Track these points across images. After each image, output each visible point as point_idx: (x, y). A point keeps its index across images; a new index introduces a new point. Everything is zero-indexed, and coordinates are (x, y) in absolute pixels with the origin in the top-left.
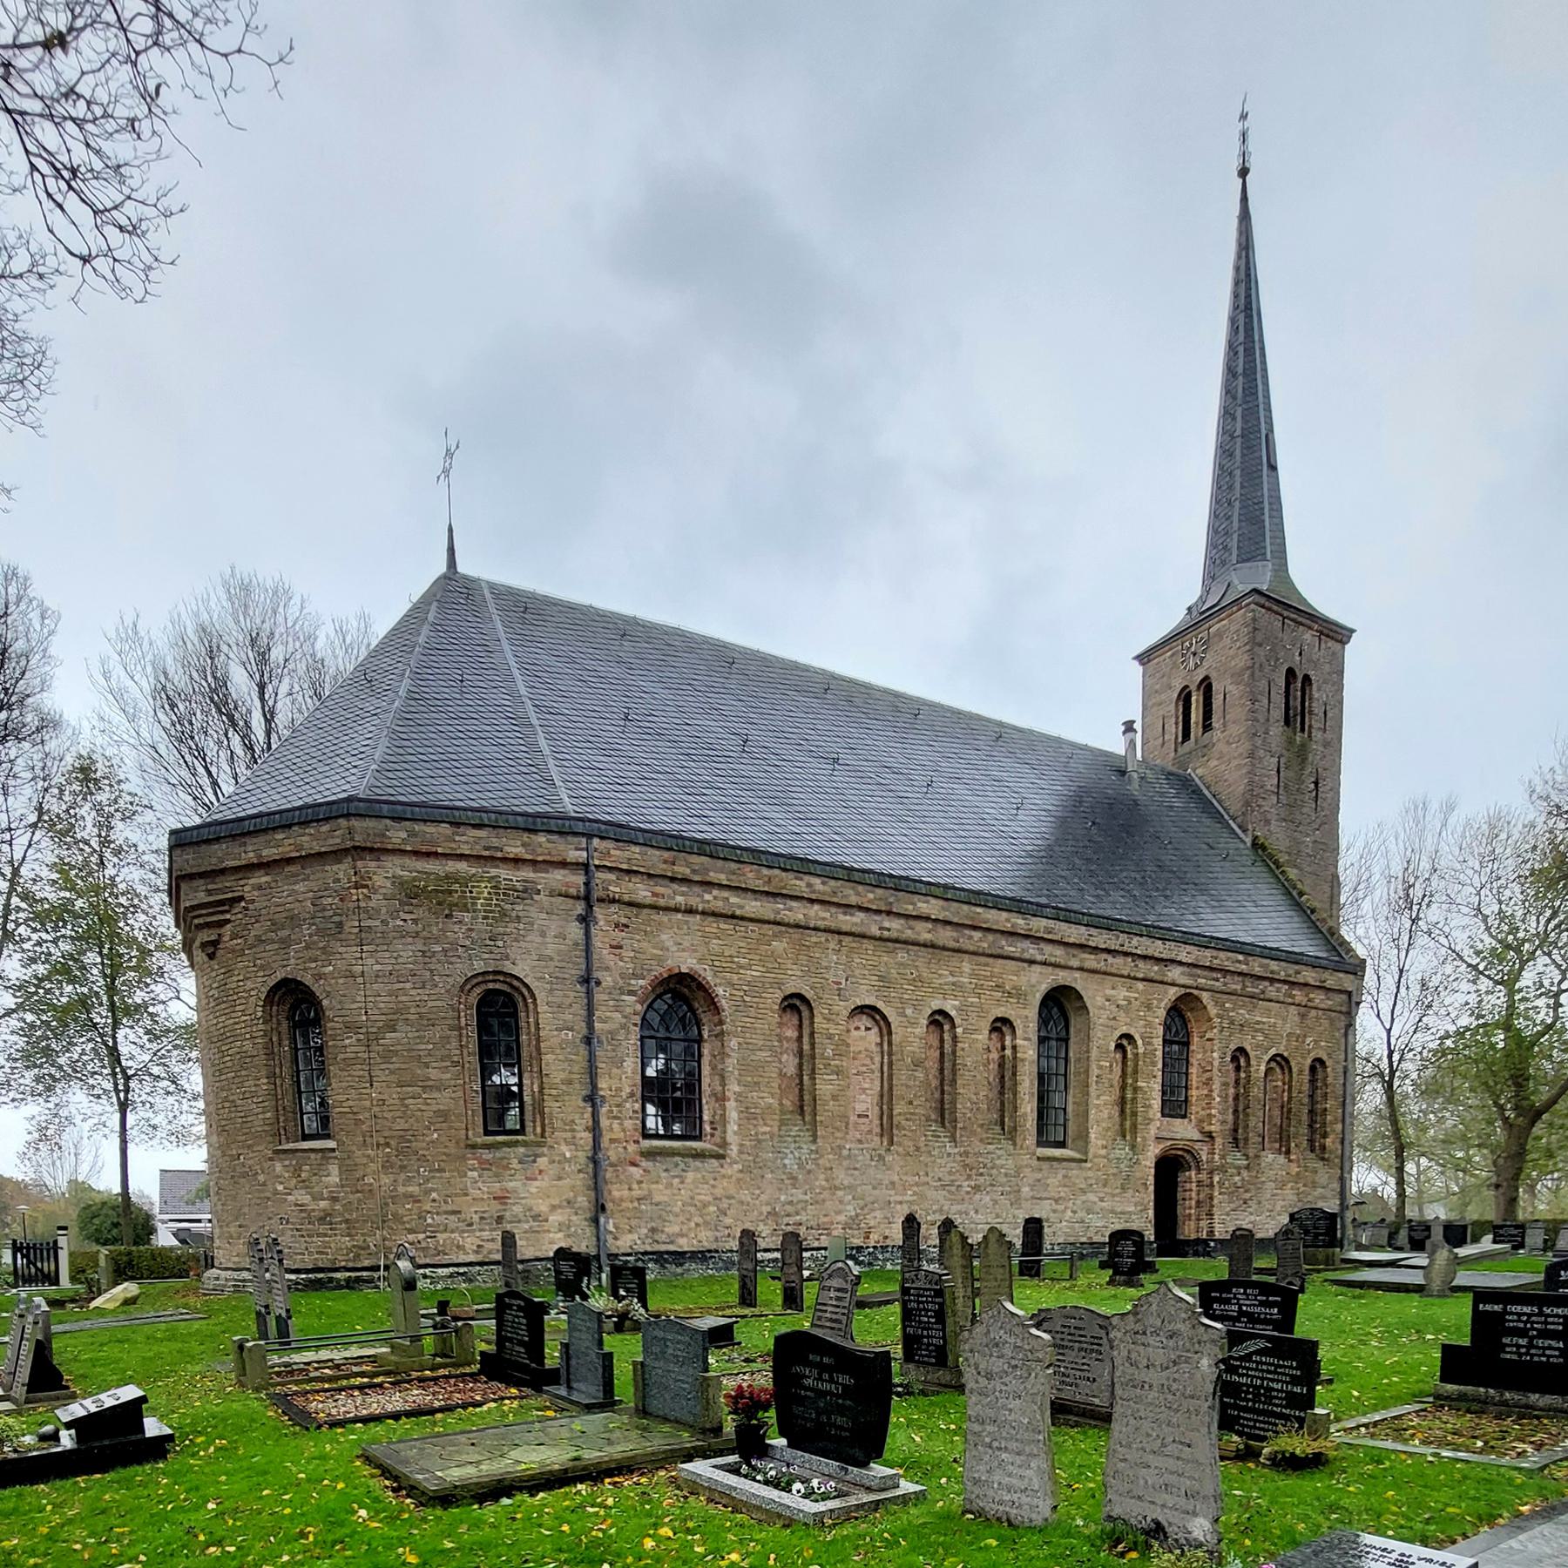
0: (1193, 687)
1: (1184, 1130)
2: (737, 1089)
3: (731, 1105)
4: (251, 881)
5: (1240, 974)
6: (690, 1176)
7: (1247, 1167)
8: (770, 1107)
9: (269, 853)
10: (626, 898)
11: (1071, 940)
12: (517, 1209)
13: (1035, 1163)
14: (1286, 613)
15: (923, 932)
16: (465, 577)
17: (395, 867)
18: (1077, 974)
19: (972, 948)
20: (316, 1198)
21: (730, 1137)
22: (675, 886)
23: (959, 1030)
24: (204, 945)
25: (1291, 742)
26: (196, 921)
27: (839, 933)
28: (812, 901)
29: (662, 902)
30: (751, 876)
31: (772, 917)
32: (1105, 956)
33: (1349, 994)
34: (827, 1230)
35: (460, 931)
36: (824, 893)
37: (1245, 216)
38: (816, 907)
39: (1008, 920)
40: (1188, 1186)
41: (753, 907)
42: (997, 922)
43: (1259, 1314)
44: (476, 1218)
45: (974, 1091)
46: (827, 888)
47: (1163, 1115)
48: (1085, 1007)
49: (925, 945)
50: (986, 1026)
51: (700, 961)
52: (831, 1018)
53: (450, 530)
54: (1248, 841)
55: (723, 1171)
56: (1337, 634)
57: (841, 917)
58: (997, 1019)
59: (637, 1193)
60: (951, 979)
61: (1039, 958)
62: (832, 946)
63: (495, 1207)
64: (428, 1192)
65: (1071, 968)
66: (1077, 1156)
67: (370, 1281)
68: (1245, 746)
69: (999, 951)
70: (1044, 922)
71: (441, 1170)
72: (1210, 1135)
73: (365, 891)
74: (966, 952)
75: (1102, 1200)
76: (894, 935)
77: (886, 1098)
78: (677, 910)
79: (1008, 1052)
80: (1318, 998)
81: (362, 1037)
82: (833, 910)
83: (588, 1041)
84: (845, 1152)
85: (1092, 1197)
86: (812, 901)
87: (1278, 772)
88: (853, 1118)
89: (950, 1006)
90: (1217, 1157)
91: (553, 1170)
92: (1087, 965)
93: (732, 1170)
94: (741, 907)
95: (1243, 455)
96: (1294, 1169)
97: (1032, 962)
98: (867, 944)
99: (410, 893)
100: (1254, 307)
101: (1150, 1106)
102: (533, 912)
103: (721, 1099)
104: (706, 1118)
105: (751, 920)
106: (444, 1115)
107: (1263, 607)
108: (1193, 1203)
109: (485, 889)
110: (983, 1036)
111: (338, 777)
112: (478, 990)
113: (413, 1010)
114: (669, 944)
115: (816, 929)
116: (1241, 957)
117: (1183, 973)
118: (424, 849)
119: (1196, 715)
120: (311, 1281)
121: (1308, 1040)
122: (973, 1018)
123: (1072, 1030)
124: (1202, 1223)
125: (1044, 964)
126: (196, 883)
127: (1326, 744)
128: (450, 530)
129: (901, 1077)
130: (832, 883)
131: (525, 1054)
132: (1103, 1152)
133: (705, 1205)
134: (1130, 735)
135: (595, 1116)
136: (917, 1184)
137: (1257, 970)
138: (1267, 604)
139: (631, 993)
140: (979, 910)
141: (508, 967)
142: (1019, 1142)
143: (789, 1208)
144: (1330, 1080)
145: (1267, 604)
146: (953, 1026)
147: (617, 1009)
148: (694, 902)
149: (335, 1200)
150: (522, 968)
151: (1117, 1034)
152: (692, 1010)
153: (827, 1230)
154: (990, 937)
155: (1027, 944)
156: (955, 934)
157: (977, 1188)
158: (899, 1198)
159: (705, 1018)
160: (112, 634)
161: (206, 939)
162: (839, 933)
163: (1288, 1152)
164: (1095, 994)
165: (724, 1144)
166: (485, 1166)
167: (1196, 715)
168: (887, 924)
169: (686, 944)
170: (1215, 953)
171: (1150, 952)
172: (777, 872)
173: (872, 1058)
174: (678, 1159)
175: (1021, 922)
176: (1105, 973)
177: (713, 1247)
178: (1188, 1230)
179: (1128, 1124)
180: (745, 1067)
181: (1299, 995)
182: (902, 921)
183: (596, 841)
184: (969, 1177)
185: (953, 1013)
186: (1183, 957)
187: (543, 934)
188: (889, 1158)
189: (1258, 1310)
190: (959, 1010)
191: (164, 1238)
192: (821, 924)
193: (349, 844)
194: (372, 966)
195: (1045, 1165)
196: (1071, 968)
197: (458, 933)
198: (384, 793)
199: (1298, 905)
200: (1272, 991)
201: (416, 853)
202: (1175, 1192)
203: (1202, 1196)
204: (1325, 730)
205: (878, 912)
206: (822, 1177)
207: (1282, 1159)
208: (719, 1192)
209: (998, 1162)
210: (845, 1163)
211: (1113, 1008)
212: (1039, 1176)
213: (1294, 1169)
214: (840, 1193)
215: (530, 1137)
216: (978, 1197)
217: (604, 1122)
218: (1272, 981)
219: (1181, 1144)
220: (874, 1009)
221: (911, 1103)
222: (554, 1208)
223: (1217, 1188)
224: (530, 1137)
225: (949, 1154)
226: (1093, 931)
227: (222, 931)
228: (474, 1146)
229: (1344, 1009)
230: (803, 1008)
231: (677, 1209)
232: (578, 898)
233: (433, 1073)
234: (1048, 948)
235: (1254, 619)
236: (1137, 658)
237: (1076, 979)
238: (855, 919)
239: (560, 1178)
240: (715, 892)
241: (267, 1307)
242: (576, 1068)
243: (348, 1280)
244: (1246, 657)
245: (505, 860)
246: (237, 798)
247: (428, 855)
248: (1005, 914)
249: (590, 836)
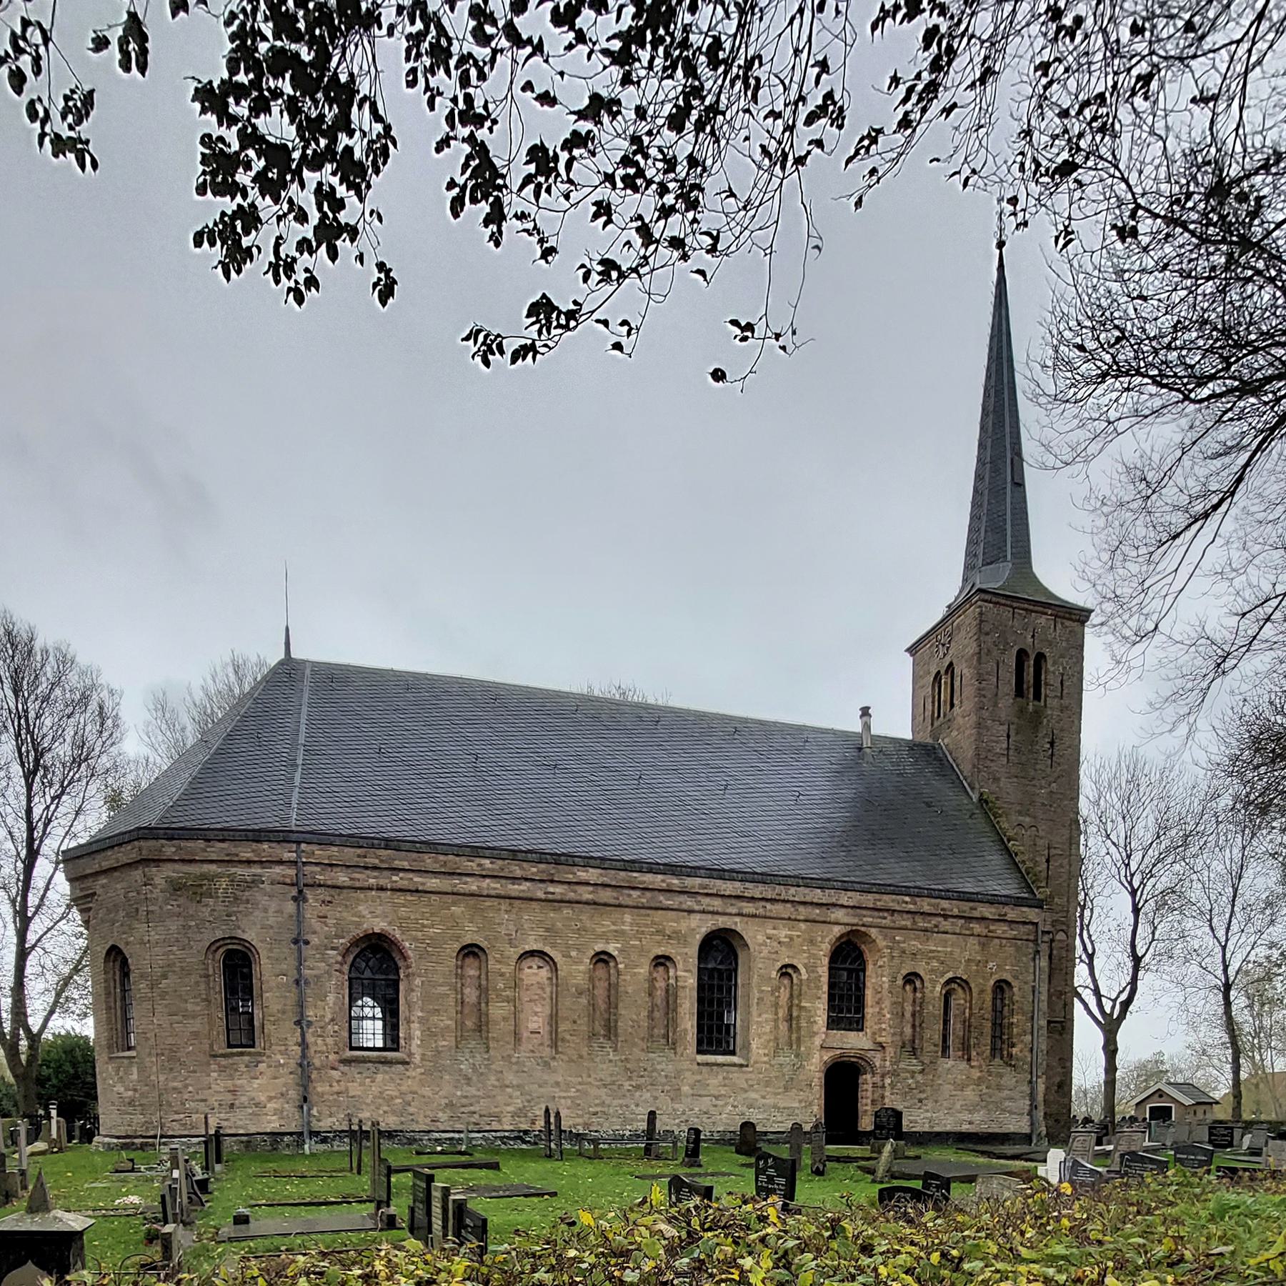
1: (854, 1041)
2: (420, 1014)
3: (415, 1026)
5: (908, 912)
6: (379, 1077)
7: (922, 1072)
8: (448, 1027)
9: (106, 865)
10: (329, 883)
11: (727, 893)
12: (244, 1099)
13: (696, 1067)
14: (1015, 605)
17: (169, 871)
18: (737, 919)
19: (631, 903)
20: (127, 1089)
21: (414, 1049)
22: (368, 872)
23: (621, 966)
25: (1022, 711)
27: (510, 898)
28: (484, 876)
29: (357, 884)
30: (429, 861)
31: (449, 889)
32: (763, 903)
34: (498, 1117)
35: (206, 911)
36: (493, 870)
37: (1001, 280)
38: (488, 881)
39: (663, 881)
41: (433, 883)
42: (653, 883)
44: (216, 1104)
45: (632, 1014)
51: (390, 923)
52: (501, 962)
54: (975, 797)
55: (408, 1074)
57: (510, 886)
59: (336, 1088)
60: (613, 928)
61: (697, 908)
62: (503, 908)
63: (229, 1097)
64: (186, 1086)
65: (730, 914)
67: (153, 1145)
68: (974, 718)
69: (658, 905)
70: (698, 881)
71: (194, 1072)
72: (882, 1047)
74: (627, 907)
75: (764, 1097)
76: (559, 897)
77: (554, 1019)
78: (371, 889)
79: (672, 981)
80: (1001, 929)
82: (503, 881)
83: (297, 982)
84: (514, 1060)
85: (753, 1095)
86: (484, 876)
87: (1008, 736)
89: (612, 948)
90: (888, 1063)
91: (270, 1072)
92: (745, 911)
94: (423, 884)
95: (991, 477)
96: (976, 1074)
97: (690, 911)
98: (534, 905)
99: (176, 888)
100: (1005, 355)
102: (258, 896)
103: (409, 1022)
104: (401, 1035)
106: (196, 1035)
107: (990, 602)
108: (869, 1101)
109: (224, 883)
110: (644, 970)
112: (221, 950)
114: (365, 913)
115: (488, 896)
116: (907, 899)
117: (848, 914)
118: (187, 858)
120: (125, 1144)
121: (991, 964)
122: (634, 957)
123: (740, 962)
125: (703, 912)
127: (1063, 709)
129: (566, 1003)
130: (500, 862)
132: (766, 1059)
133: (392, 1098)
134: (865, 718)
135: (303, 1035)
136: (580, 1084)
137: (926, 908)
138: (994, 599)
139: (333, 949)
140: (635, 874)
141: (239, 934)
142: (679, 1050)
143: (464, 1101)
144: (1016, 998)
145: (994, 599)
148: (382, 882)
149: (135, 1090)
150: (250, 935)
153: (498, 1117)
154: (648, 894)
155: (683, 898)
156: (615, 894)
157: (638, 1087)
159: (401, 963)
160: (151, 707)
162: (510, 898)
163: (969, 1060)
164: (755, 935)
165: (410, 1054)
166: (222, 1069)
168: (551, 890)
169: (378, 912)
170: (877, 896)
171: (808, 899)
172: (451, 857)
173: (543, 989)
174: (370, 1065)
175: (676, 882)
176: (765, 917)
177: (399, 1128)
179: (794, 1036)
180: (426, 998)
181: (977, 928)
182: (566, 887)
183: (303, 846)
184: (630, 1078)
185: (615, 953)
186: (844, 901)
187: (266, 910)
188: (553, 1064)
190: (620, 951)
192: (493, 893)
194: (154, 936)
195: (705, 1069)
196: (730, 914)
197: (205, 912)
199: (1007, 849)
200: (946, 925)
201: (183, 861)
203: (876, 1095)
204: (1061, 698)
206: (493, 1078)
207: (963, 1065)
208: (404, 1088)
209: (659, 1067)
210: (515, 1067)
211: (775, 944)
212: (699, 1077)
213: (976, 1074)
214: (509, 1090)
215: (257, 1049)
216: (638, 1094)
217: (310, 1039)
219: (852, 1053)
221: (575, 1022)
222: (270, 1099)
223: (888, 1088)
224: (257, 1049)
225: (610, 1061)
226: (748, 885)
228: (215, 1056)
229: (1032, 937)
230: (480, 954)
231: (368, 1101)
232: (293, 885)
233: (190, 1007)
234: (706, 900)
235: (981, 614)
236: (907, 650)
237: (736, 923)
238: (522, 888)
239: (275, 1078)
240: (401, 875)
242: (289, 1002)
243: (142, 1144)
244: (975, 645)
245: (240, 862)
247: (191, 861)
248: (660, 877)
249: (299, 843)
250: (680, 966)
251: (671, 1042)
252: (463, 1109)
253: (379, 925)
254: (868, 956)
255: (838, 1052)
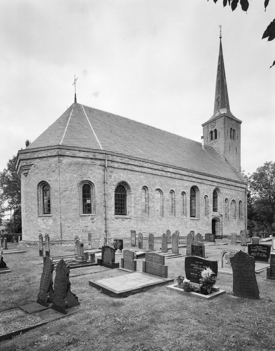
0: (213, 131)
4: (36, 161)
9: (40, 156)
15: (169, 175)
16: (78, 104)
23: (176, 194)
24: (24, 174)
26: (23, 169)
27: (153, 174)
28: (148, 168)
29: (120, 167)
33: (246, 188)
38: (149, 169)
40: (217, 225)
43: (262, 251)
46: (151, 166)
47: (213, 211)
48: (199, 190)
49: (169, 177)
50: (180, 193)
53: (75, 95)
56: (240, 122)
58: (183, 192)
66: (198, 219)
68: (224, 142)
73: (60, 164)
76: (163, 175)
81: (59, 193)
82: (152, 170)
86: (148, 168)
88: (156, 211)
93: (132, 222)
101: (211, 209)
105: (137, 171)
111: (54, 141)
113: (70, 188)
116: (226, 181)
119: (214, 136)
123: (196, 194)
124: (220, 233)
126: (24, 161)
128: (75, 95)
131: (92, 197)
146: (174, 193)
147: (111, 188)
151: (205, 195)
152: (125, 189)
154: (181, 176)
158: (165, 227)
161: (25, 172)
167: (214, 136)
168: (162, 173)
178: (218, 234)
185: (174, 190)
189: (262, 250)
191: (246, 250)
192: (150, 173)
193: (57, 154)
198: (65, 144)
202: (215, 226)
205: (161, 170)
218: (232, 186)
219: (216, 217)
220: (160, 189)
227: (29, 171)
240: (130, 166)
241: (43, 249)
246: (33, 144)
250: (187, 195)
251: (186, 215)
252: (143, 231)
253: (122, 179)
254: (218, 194)
255: (214, 217)
